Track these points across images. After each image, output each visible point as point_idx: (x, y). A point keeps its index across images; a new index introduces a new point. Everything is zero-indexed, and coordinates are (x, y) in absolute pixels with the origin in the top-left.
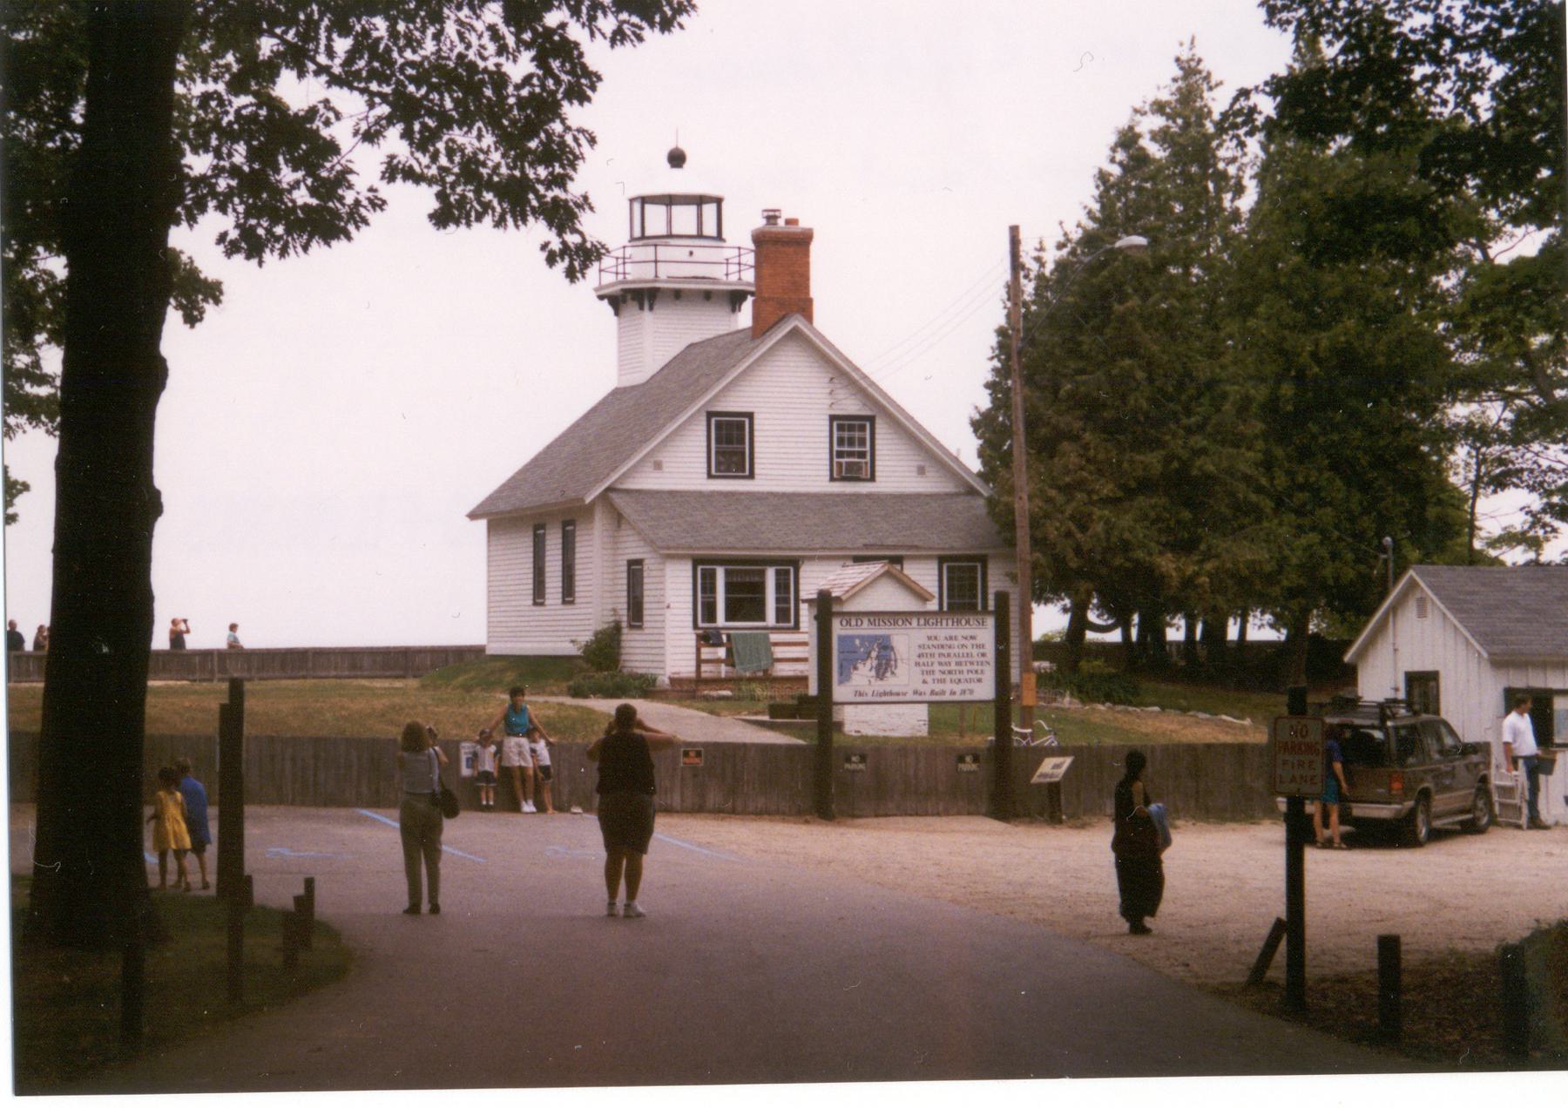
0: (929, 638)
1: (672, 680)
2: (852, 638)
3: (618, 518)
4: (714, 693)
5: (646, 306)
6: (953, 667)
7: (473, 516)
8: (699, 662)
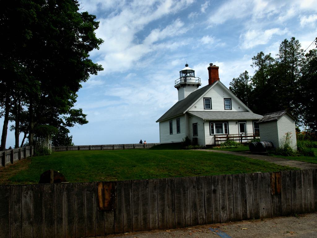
7: (157, 122)
8: (215, 141)
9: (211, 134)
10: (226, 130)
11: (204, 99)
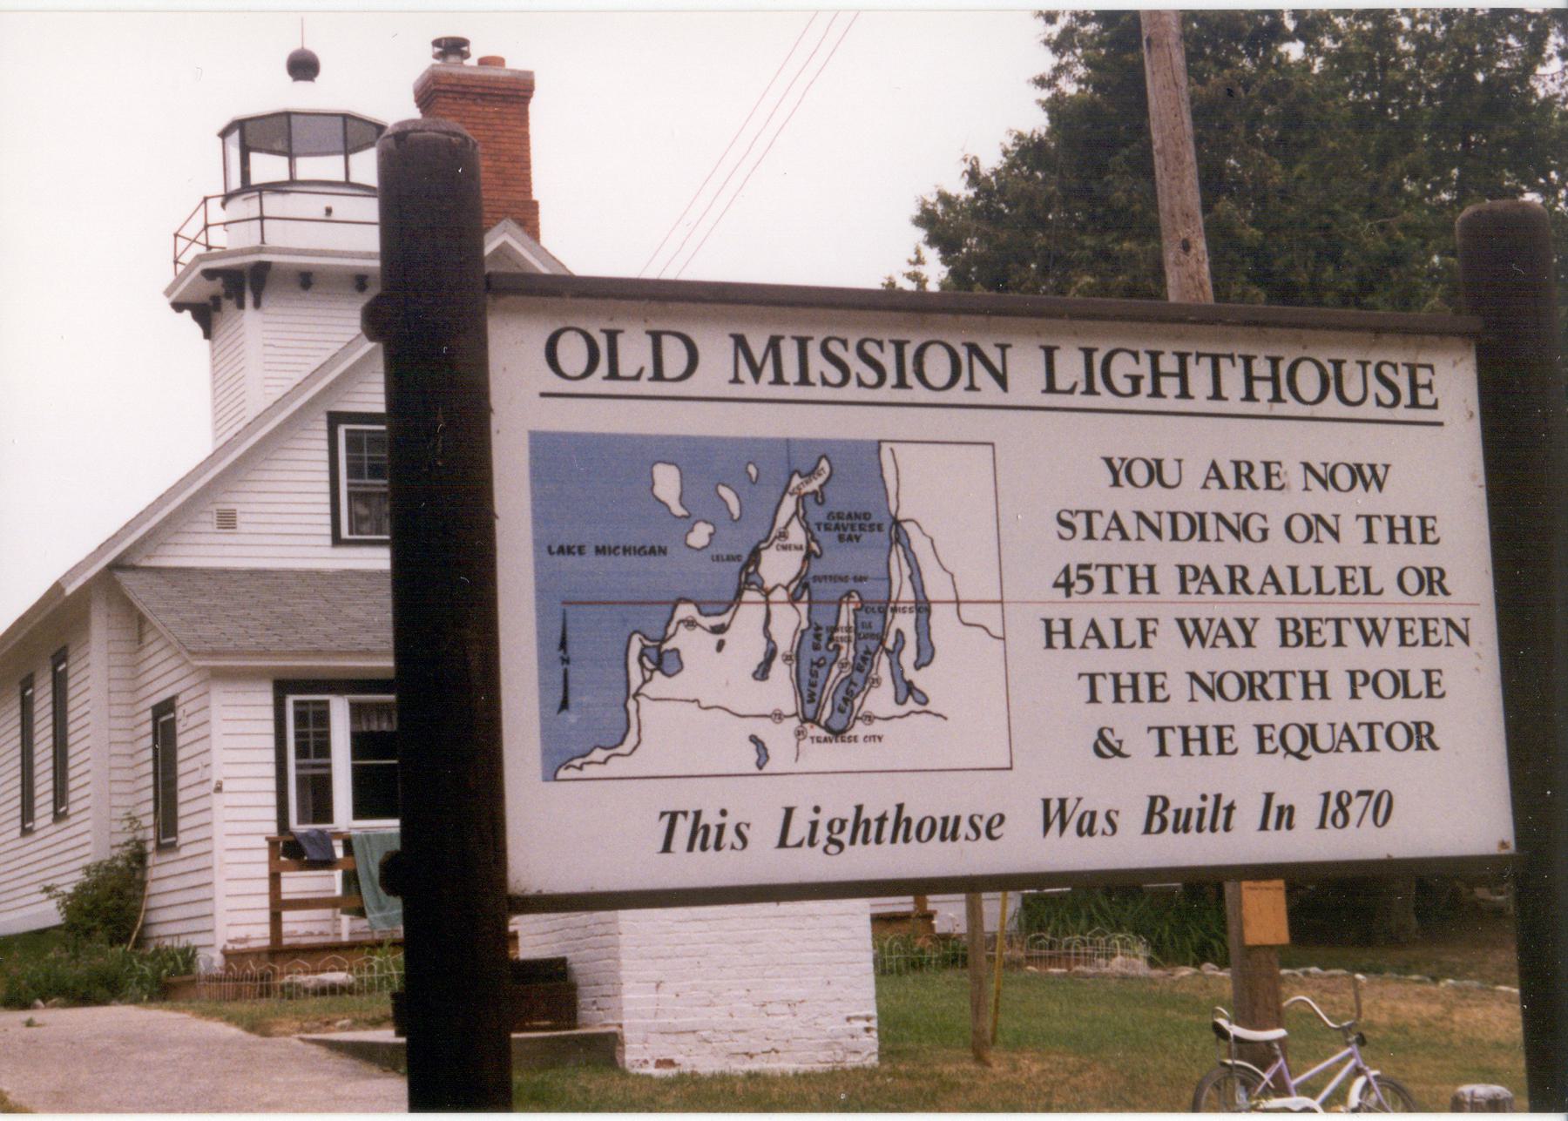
0: (1119, 472)
1: (227, 954)
2: (644, 453)
3: (137, 624)
4: (309, 980)
5: (249, 300)
6: (1267, 654)
8: (278, 906)
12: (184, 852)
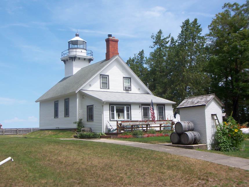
5: (73, 61)
7: (36, 102)
9: (111, 120)
10: (128, 115)
11: (100, 76)
12: (94, 122)
